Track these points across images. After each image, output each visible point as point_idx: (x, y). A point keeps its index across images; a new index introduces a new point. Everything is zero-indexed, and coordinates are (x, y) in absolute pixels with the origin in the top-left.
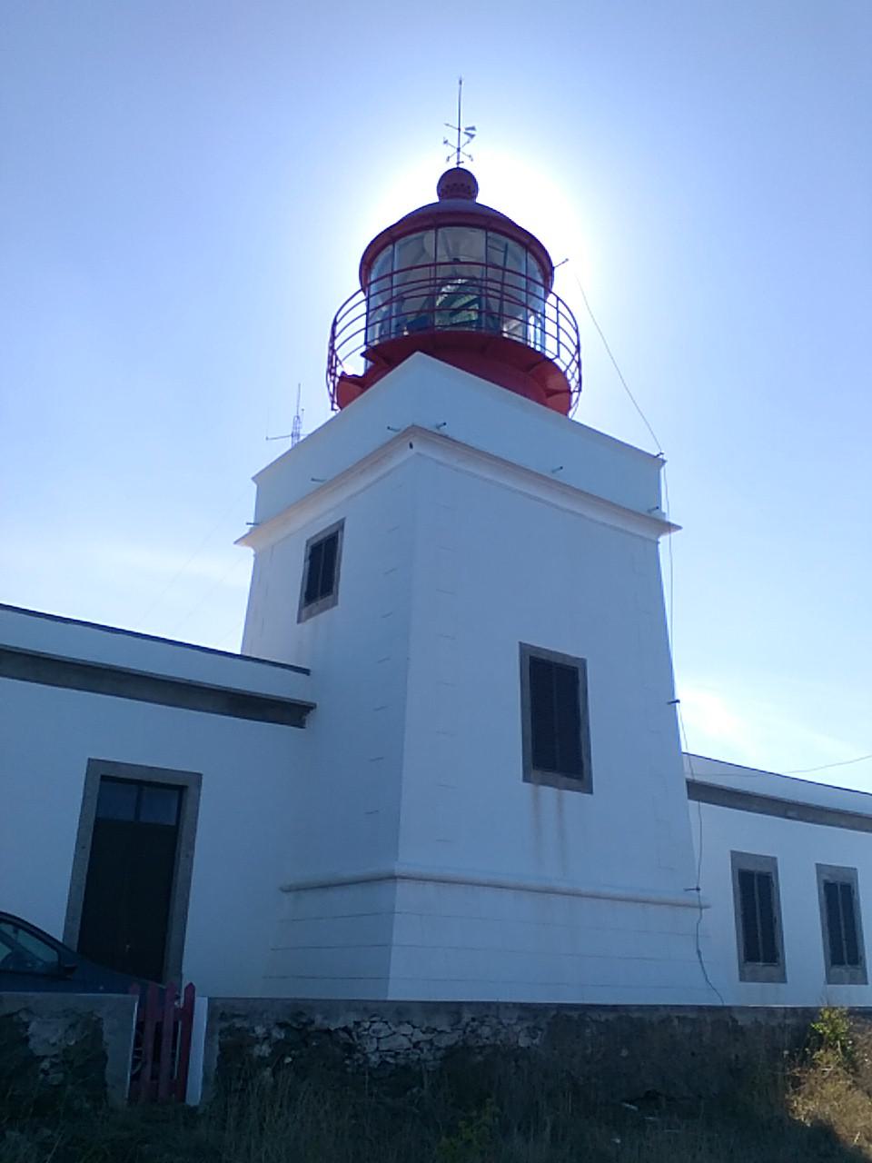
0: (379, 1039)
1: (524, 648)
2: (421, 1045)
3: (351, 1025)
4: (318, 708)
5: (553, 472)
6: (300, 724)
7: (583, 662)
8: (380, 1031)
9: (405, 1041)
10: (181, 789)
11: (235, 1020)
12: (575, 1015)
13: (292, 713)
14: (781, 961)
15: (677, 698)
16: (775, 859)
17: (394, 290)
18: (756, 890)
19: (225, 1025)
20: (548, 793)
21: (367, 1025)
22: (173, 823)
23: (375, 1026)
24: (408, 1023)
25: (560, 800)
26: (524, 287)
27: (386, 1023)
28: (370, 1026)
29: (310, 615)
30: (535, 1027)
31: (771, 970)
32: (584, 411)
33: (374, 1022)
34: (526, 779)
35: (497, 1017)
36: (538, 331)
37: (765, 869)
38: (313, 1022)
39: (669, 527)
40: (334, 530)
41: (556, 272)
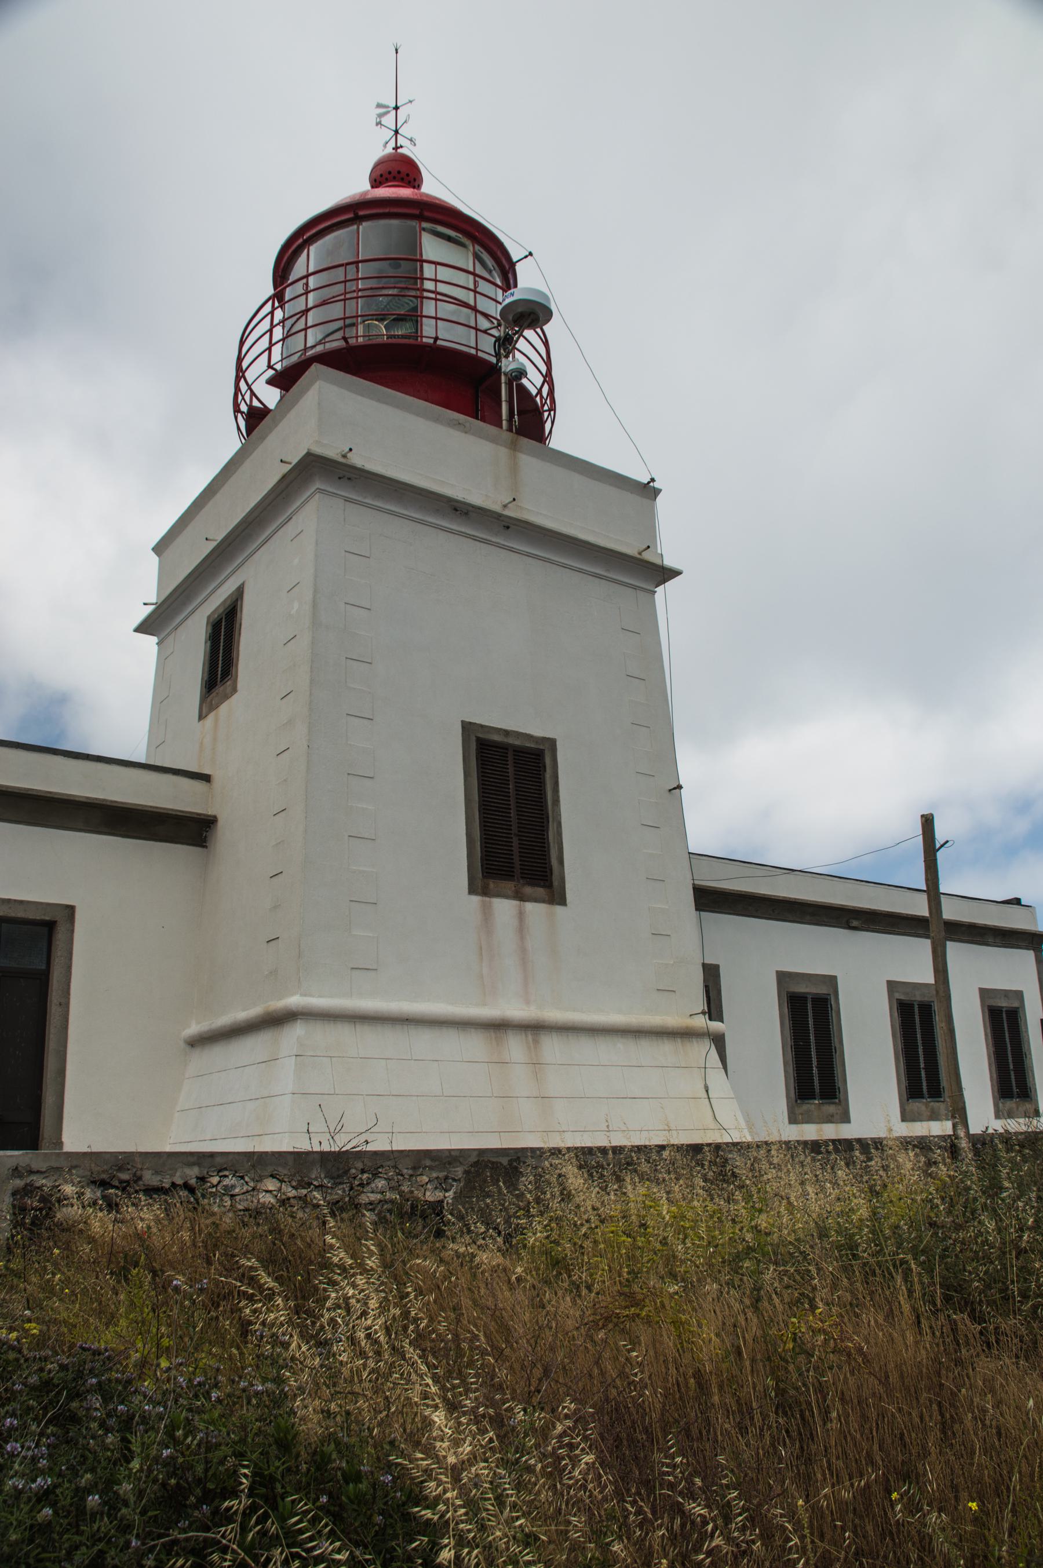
0: (232, 1196)
1: (467, 727)
2: (292, 1200)
3: (193, 1182)
4: (221, 823)
5: (505, 506)
6: (716, 968)
7: (552, 743)
8: (233, 1187)
9: (269, 1199)
10: (48, 927)
11: (34, 1177)
12: (505, 1161)
13: (194, 830)
14: (842, 1098)
15: (150, 642)
16: (835, 977)
17: (311, 296)
18: (810, 1020)
19: (19, 1183)
20: (504, 908)
21: (215, 1180)
22: (44, 967)
23: (226, 1182)
24: (272, 1176)
25: (521, 915)
26: (472, 286)
27: (242, 1178)
28: (219, 1182)
29: (212, 708)
30: (446, 1178)
31: (831, 1109)
32: (566, 434)
33: (226, 1176)
34: (472, 891)
35: (395, 1167)
36: (340, 288)
37: (821, 990)
38: (140, 1178)
39: (666, 574)
40: (234, 598)
41: (518, 267)
